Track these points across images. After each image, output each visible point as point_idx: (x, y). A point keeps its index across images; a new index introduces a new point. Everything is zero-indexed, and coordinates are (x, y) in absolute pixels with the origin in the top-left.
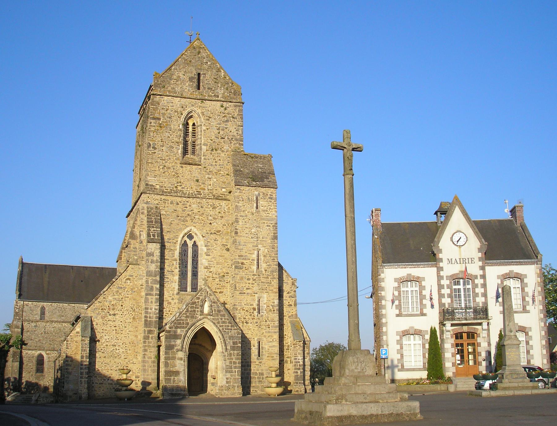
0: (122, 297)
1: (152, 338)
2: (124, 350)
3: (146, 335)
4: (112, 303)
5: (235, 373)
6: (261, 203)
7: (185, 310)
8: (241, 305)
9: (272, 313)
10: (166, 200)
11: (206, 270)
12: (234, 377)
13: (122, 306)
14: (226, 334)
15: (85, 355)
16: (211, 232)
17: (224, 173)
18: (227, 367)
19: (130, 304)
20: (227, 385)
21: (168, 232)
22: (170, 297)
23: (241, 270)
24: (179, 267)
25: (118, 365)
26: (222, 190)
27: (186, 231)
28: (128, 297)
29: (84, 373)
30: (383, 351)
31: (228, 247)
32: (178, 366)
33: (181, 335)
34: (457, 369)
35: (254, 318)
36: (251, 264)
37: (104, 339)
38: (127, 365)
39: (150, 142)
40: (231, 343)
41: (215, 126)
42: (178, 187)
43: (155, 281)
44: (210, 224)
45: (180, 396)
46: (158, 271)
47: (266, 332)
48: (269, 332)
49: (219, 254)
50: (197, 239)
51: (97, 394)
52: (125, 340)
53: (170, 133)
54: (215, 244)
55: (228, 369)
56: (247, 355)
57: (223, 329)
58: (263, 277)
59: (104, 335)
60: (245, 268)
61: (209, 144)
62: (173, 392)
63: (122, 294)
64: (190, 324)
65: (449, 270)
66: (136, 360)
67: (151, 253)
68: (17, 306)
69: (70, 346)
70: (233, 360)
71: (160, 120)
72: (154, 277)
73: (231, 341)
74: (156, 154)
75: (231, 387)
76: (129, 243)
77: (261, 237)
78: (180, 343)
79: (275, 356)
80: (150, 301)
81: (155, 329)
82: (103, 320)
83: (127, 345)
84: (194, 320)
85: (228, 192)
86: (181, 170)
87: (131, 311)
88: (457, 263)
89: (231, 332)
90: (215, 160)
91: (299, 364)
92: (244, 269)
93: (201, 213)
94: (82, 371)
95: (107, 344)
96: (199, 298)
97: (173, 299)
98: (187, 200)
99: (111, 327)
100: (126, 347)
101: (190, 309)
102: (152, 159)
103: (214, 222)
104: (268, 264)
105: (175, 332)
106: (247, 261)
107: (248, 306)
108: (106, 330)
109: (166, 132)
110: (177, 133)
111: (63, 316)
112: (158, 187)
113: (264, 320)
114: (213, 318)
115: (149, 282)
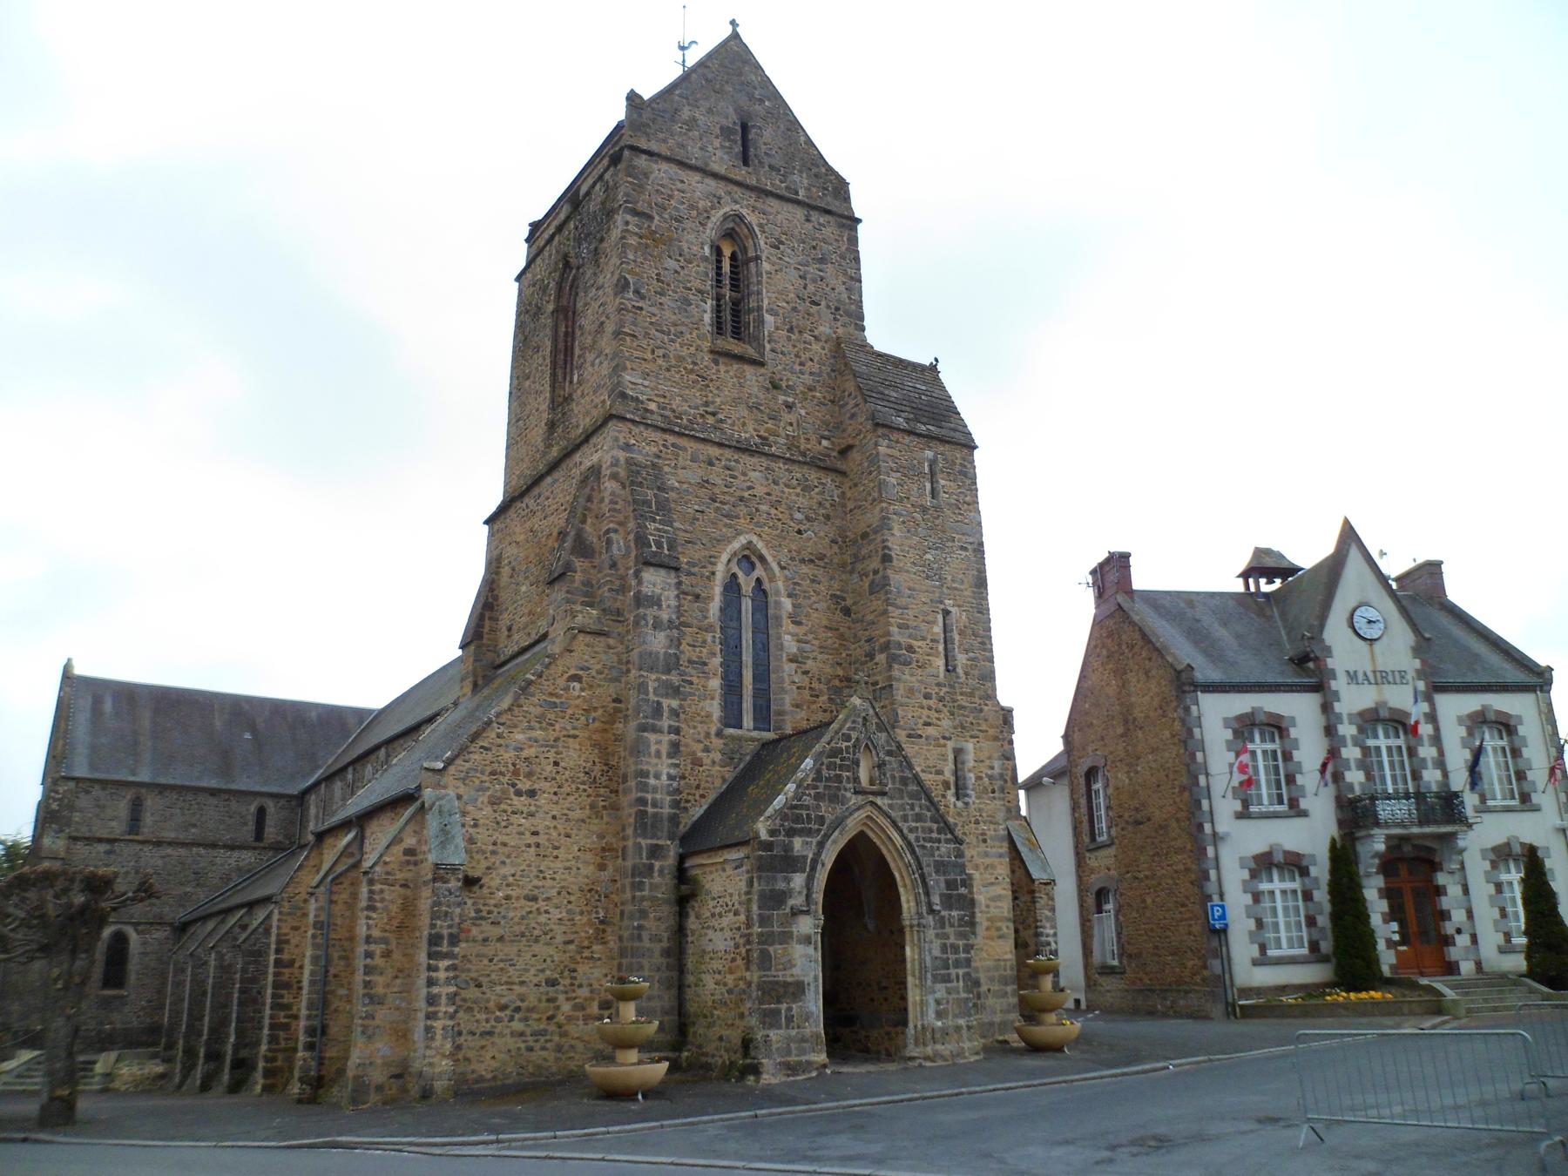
0: (556, 734)
1: (661, 871)
2: (564, 914)
3: (645, 861)
4: (525, 753)
6: (942, 482)
9: (989, 799)
10: (680, 448)
11: (794, 665)
13: (556, 764)
15: (445, 932)
16: (801, 557)
17: (824, 397)
19: (582, 759)
20: (939, 1024)
21: (689, 542)
22: (699, 741)
23: (907, 670)
24: (721, 650)
25: (544, 966)
26: (820, 444)
27: (736, 545)
28: (575, 737)
29: (444, 998)
30: (1216, 908)
31: (849, 602)
32: (799, 963)
33: (805, 857)
34: (1398, 953)
36: (932, 652)
37: (498, 875)
38: (573, 966)
39: (627, 276)
40: (943, 885)
41: (795, 268)
42: (707, 416)
44: (799, 532)
47: (979, 854)
48: (986, 855)
49: (825, 622)
50: (764, 574)
51: (473, 1072)
52: (565, 880)
53: (679, 261)
54: (814, 591)
57: (917, 839)
58: (961, 694)
59: (498, 863)
61: (781, 311)
63: (557, 727)
64: (828, 822)
65: (1353, 699)
66: (600, 947)
67: (652, 597)
68: (57, 792)
69: (383, 900)
71: (652, 222)
74: (644, 312)
75: (951, 1031)
76: (568, 567)
77: (949, 578)
78: (804, 884)
79: (1003, 925)
80: (653, 748)
81: (669, 842)
82: (495, 811)
83: (572, 898)
84: (839, 809)
85: (837, 448)
86: (714, 371)
88: (1370, 683)
90: (800, 357)
91: (1048, 948)
92: (914, 665)
93: (774, 498)
94: (435, 990)
95: (510, 892)
97: (707, 750)
98: (736, 457)
99: (523, 834)
100: (569, 902)
101: (825, 773)
102: (634, 324)
103: (809, 529)
104: (971, 654)
105: (788, 848)
107: (930, 776)
108: (505, 845)
109: (670, 257)
110: (698, 266)
111: (194, 826)
112: (653, 406)
113: (973, 820)
114: (890, 802)
115: (651, 690)
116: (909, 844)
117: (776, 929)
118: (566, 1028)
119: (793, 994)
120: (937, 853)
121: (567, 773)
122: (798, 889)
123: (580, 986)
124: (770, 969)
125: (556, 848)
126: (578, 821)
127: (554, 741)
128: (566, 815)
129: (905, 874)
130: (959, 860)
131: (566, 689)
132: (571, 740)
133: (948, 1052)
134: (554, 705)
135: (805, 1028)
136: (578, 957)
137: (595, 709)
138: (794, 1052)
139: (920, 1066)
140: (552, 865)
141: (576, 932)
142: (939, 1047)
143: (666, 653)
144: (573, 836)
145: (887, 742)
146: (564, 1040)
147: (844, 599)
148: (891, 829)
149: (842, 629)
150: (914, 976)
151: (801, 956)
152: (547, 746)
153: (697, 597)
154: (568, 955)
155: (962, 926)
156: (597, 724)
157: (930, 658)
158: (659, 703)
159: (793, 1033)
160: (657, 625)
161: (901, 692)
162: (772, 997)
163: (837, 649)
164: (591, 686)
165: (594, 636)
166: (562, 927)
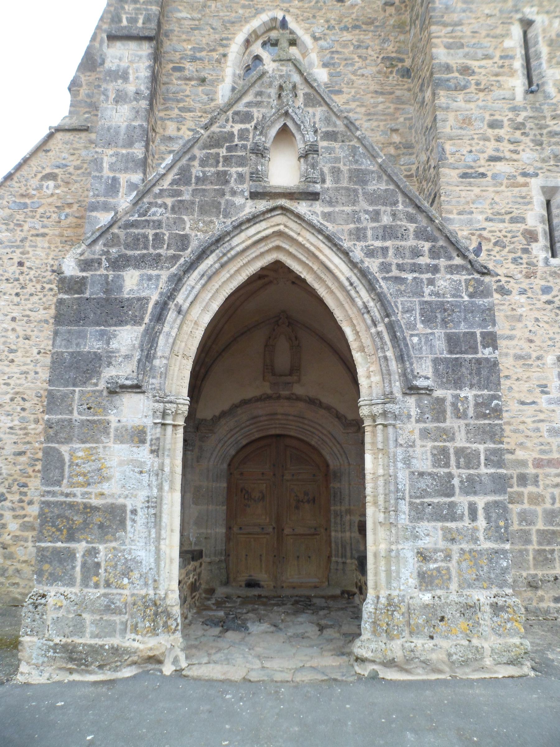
0: (23, 235)
2: (16, 422)
5: (473, 516)
7: (170, 177)
8: (470, 222)
12: (464, 546)
13: (21, 264)
14: (401, 293)
16: (342, 25)
18: (422, 484)
19: (51, 257)
20: (427, 598)
23: (460, 96)
28: (44, 235)
32: (117, 474)
35: (535, 273)
38: (24, 480)
40: (440, 345)
43: (127, 161)
45: (116, 669)
46: (141, 126)
52: (20, 385)
54: (360, 57)
55: (424, 493)
56: (515, 431)
57: (385, 267)
60: (478, 84)
62: (78, 640)
63: (26, 227)
67: (117, 71)
70: (453, 439)
72: (124, 147)
73: (440, 332)
83: (27, 405)
87: (50, 282)
89: (431, 282)
92: (472, 88)
96: (246, 117)
100: (23, 409)
101: (196, 170)
106: (483, 63)
107: (501, 226)
114: (328, 209)
115: (105, 165)
116: (364, 274)
117: (75, 415)
118: (12, 549)
119: (101, 526)
120: (427, 290)
121: (32, 273)
122: (124, 351)
123: (31, 503)
124: (59, 483)
125: (11, 351)
126: (41, 321)
127: (22, 241)
128: (28, 316)
129: (361, 327)
130: (479, 301)
131: (39, 188)
132: (39, 239)
133: (443, 656)
134: (25, 205)
135: (122, 587)
136: (30, 470)
137: (70, 205)
138: (90, 629)
139: (374, 676)
140: (7, 369)
141: (29, 443)
142: (420, 642)
143: (128, 127)
144: (33, 338)
145: (327, 120)
146: (9, 562)
147: (402, 60)
148: (327, 251)
149: (398, 93)
150: (375, 503)
151: (121, 464)
152: (12, 247)
153: (203, 80)
154: (19, 467)
155: (485, 416)
156: (71, 220)
157: (499, 78)
158: (115, 179)
159: (93, 593)
160: (120, 98)
161: (451, 121)
162: (60, 530)
163: (392, 114)
164: (68, 183)
165: (75, 133)
166: (13, 436)
